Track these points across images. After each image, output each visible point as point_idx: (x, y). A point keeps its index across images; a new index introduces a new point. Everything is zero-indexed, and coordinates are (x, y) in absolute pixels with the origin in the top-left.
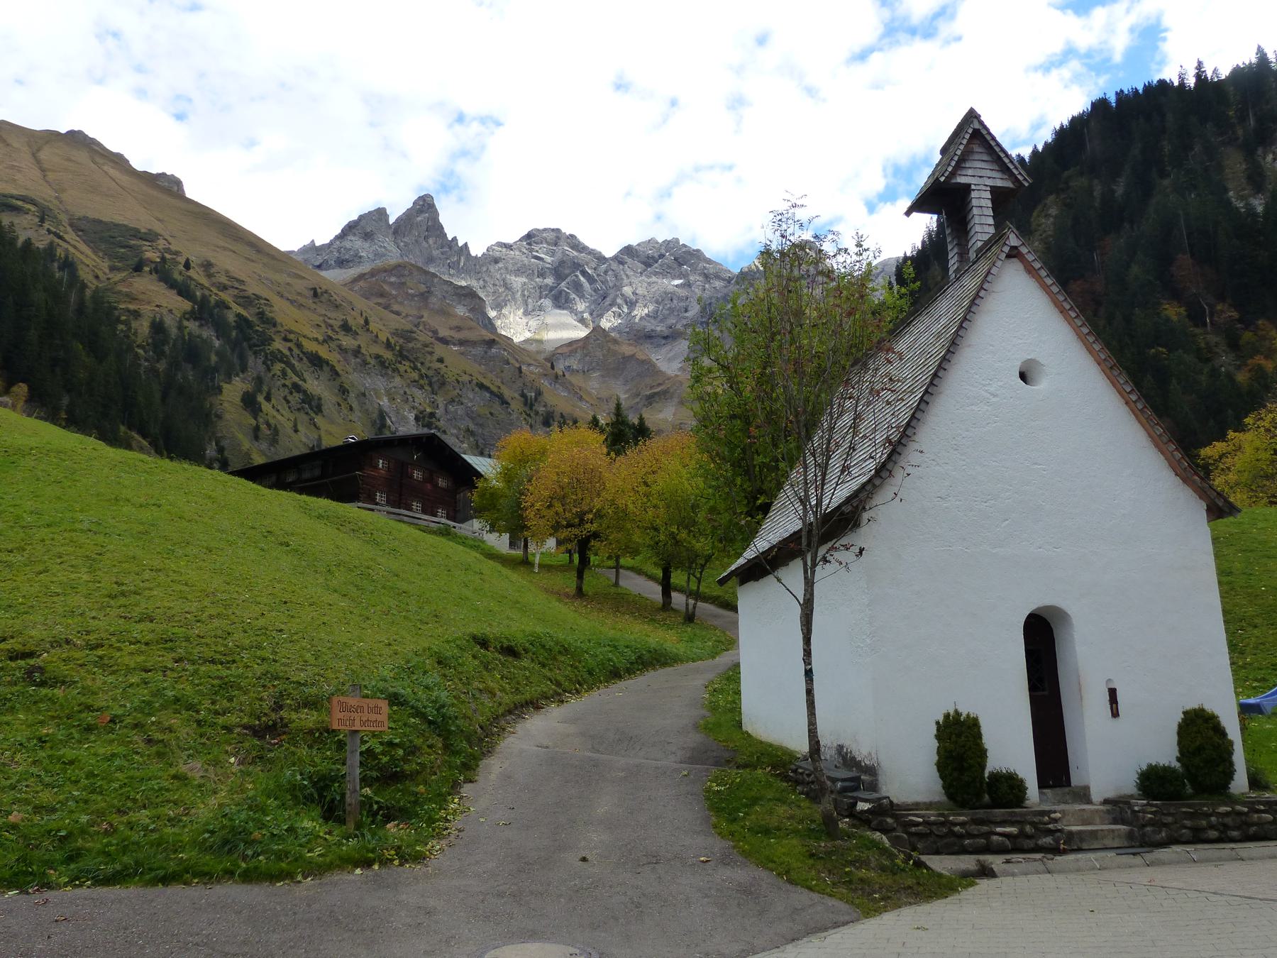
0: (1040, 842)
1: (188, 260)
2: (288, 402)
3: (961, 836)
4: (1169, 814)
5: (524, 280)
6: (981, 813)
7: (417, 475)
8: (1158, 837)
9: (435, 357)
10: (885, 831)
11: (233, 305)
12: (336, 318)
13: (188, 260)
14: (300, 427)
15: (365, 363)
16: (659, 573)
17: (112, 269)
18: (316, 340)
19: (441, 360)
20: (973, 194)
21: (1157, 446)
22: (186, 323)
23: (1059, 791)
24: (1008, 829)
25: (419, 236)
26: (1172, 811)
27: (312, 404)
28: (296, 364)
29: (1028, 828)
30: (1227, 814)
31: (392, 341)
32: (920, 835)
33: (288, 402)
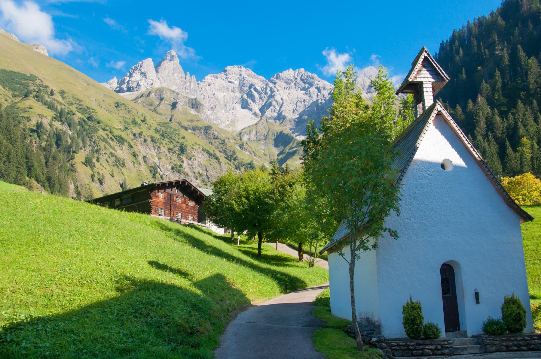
0: (443, 352)
1: (52, 90)
2: (108, 162)
3: (412, 350)
4: (497, 341)
5: (224, 94)
6: (420, 342)
7: (178, 200)
8: (492, 349)
9: (181, 136)
10: (382, 348)
11: (77, 113)
12: (129, 118)
13: (52, 90)
14: (115, 174)
15: (145, 141)
16: (297, 245)
17: (15, 96)
18: (120, 129)
19: (184, 138)
20: (424, 86)
21: (499, 193)
22: (54, 123)
23: (454, 333)
24: (430, 347)
25: (169, 73)
26: (498, 339)
27: (119, 163)
28: (111, 142)
29: (439, 347)
30: (521, 340)
31: (159, 129)
32: (396, 350)
33: (108, 162)
